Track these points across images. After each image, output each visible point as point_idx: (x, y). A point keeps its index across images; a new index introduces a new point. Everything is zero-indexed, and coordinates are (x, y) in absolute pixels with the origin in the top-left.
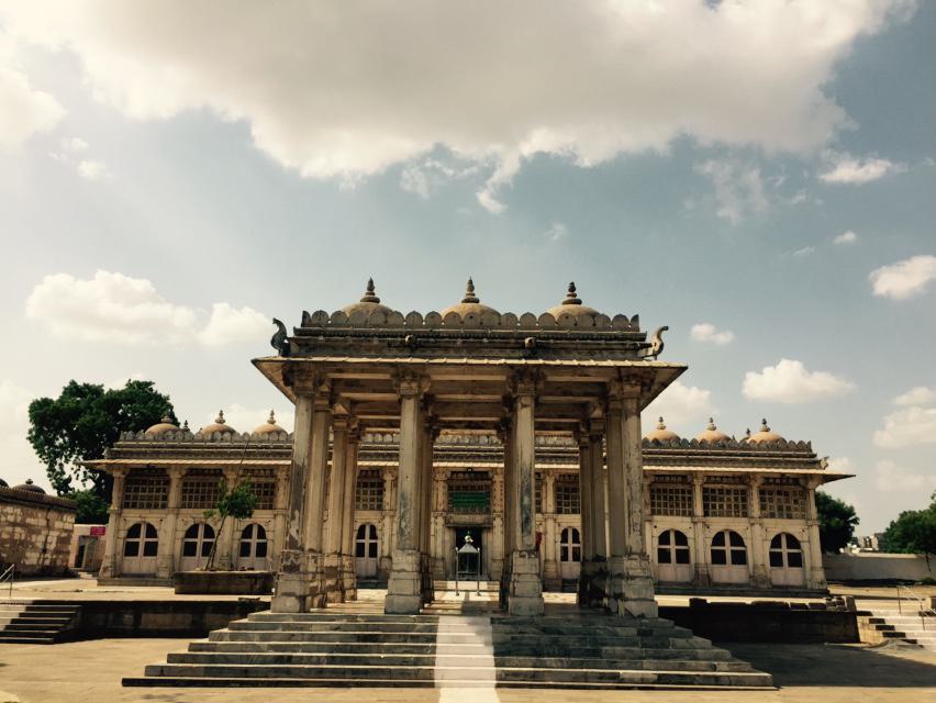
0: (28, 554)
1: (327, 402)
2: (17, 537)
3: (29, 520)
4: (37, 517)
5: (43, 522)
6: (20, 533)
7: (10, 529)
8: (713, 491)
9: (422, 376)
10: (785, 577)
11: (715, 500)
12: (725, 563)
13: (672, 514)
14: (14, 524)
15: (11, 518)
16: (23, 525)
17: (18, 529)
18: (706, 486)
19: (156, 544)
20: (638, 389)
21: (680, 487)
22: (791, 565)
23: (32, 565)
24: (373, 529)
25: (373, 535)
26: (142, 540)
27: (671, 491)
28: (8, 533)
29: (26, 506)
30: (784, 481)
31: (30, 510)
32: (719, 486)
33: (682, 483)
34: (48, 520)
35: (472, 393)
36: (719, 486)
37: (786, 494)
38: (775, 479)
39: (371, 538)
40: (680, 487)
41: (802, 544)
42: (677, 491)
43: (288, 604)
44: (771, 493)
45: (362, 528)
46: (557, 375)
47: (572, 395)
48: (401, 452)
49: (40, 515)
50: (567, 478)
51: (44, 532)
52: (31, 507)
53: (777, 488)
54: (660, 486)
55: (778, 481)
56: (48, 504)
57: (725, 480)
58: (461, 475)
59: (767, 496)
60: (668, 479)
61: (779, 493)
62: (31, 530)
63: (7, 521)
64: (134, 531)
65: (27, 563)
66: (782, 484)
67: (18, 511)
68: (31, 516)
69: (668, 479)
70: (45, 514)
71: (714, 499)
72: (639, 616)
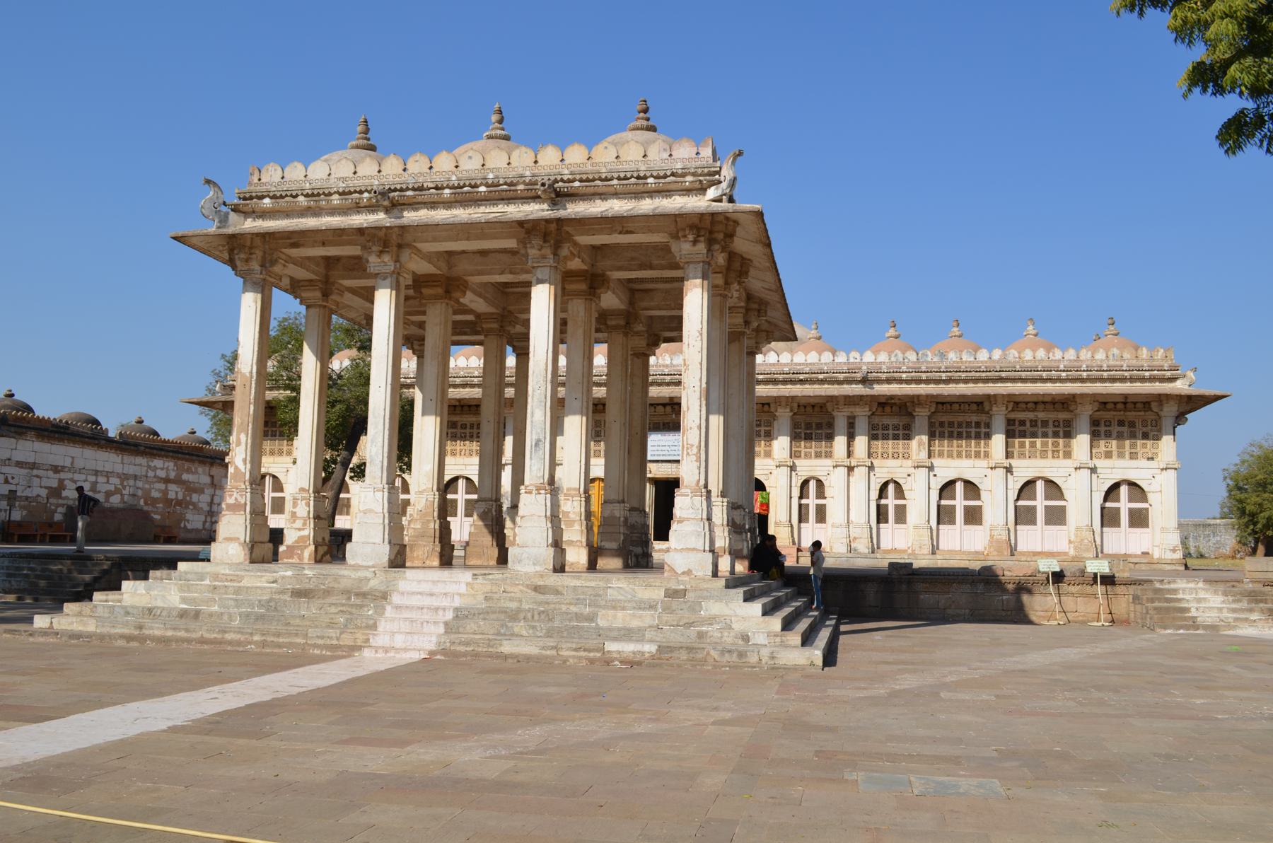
0: (189, 516)
1: (318, 294)
2: (172, 495)
3: (185, 477)
4: (196, 473)
5: (207, 480)
6: (174, 491)
7: (162, 486)
8: (1022, 423)
9: (400, 246)
10: (571, 543)
11: (1024, 437)
12: (1035, 524)
13: (959, 456)
14: (167, 481)
15: (162, 474)
16: (179, 481)
17: (172, 487)
18: (1012, 416)
19: (1062, 510)
20: (702, 247)
21: (974, 418)
22: (1049, 522)
23: (197, 530)
24: (820, 483)
25: (821, 493)
26: (1040, 502)
27: (960, 425)
28: (160, 491)
29: (179, 459)
30: (1129, 406)
31: (187, 465)
32: (1031, 415)
33: (977, 412)
34: (212, 477)
35: (511, 273)
36: (1031, 415)
37: (1132, 424)
38: (1115, 404)
39: (896, 498)
40: (974, 418)
41: (1149, 496)
42: (968, 424)
43: (231, 552)
44: (1108, 423)
45: (805, 483)
46: (587, 233)
47: (651, 268)
48: (684, 379)
49: (200, 470)
50: (809, 409)
51: (209, 491)
52: (187, 460)
53: (1119, 415)
54: (946, 418)
55: (1120, 406)
56: (211, 457)
57: (1041, 407)
58: (660, 409)
59: (1102, 429)
60: (956, 407)
61: (1121, 423)
62: (190, 488)
63: (155, 476)
64: (1027, 487)
65: (189, 526)
66: (1125, 410)
67: (171, 465)
68: (189, 471)
69: (956, 407)
70: (207, 469)
71: (1023, 435)
72: (684, 573)
